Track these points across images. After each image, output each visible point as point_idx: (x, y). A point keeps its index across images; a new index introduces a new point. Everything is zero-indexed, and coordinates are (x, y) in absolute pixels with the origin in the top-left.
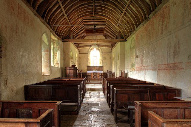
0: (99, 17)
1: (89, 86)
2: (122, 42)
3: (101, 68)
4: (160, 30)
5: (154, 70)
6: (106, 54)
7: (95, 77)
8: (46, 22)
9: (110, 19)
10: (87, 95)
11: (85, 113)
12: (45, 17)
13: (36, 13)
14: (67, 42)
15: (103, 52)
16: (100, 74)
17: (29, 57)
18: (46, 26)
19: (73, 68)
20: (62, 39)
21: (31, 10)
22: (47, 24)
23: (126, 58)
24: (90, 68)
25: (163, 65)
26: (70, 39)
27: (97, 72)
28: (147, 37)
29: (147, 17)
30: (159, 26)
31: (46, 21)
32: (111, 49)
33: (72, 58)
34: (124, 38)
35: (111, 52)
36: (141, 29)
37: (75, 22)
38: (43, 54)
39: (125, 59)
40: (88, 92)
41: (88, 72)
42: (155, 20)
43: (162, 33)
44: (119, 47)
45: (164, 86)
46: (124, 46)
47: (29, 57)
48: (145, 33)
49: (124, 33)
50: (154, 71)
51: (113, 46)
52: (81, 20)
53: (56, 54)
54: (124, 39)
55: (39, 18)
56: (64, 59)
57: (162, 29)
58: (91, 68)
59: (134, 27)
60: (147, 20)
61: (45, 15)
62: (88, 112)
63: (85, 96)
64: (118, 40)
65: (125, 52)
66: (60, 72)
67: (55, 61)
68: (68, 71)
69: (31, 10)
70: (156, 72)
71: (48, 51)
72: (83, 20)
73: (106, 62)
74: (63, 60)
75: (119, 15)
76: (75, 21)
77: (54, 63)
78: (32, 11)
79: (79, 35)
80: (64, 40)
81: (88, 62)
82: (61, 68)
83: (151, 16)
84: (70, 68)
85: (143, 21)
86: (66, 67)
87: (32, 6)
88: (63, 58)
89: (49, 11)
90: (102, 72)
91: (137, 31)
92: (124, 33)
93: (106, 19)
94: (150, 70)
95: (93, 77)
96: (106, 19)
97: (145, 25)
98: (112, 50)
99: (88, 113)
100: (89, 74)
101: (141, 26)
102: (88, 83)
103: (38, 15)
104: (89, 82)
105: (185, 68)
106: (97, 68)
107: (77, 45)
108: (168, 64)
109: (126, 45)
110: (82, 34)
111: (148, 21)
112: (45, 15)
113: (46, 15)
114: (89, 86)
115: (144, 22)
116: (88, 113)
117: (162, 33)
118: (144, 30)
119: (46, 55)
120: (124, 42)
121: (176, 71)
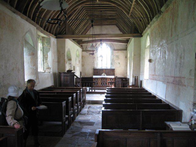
0: (105, 3)
1: (89, 97)
2: (137, 38)
3: (111, 71)
4: (170, 31)
5: (164, 82)
6: (120, 52)
7: (104, 84)
8: (29, 19)
9: (119, 5)
10: (85, 110)
11: (72, 135)
12: (28, 12)
13: (15, 10)
14: (62, 39)
15: (116, 48)
16: (110, 80)
17: (6, 67)
18: (30, 23)
19: (69, 75)
20: (55, 35)
21: (8, 8)
22: (32, 21)
23: (141, 60)
24: (97, 72)
25: (171, 77)
26: (66, 34)
27: (106, 76)
28: (159, 37)
29: (159, 9)
30: (169, 25)
31: (29, 17)
32: (127, 45)
33: (70, 59)
34: (140, 32)
35: (127, 48)
36: (154, 24)
37: (72, 12)
38: (27, 58)
39: (140, 61)
40: (88, 106)
41: (94, 77)
42: (166, 15)
43: (172, 35)
44: (133, 44)
45: (168, 104)
46: (140, 42)
47: (6, 67)
48: (158, 30)
49: (138, 24)
50: (164, 84)
51: (127, 41)
52: (81, 8)
53: (46, 57)
54: (139, 33)
55: (19, 15)
56: (59, 62)
57: (172, 30)
58: (99, 70)
59: (148, 20)
60: (160, 14)
61: (28, 10)
62: (76, 133)
63: (81, 112)
64: (132, 35)
65: (140, 52)
66: (53, 79)
67: (46, 65)
68: (62, 77)
69: (9, 9)
70: (166, 85)
71: (34, 54)
72: (84, 7)
73: (119, 63)
74: (56, 63)
75: (130, 2)
76: (72, 10)
77: (43, 68)
78: (10, 10)
79: (81, 27)
80: (58, 35)
81: (94, 62)
82: (54, 74)
83: (163, 9)
84: (65, 75)
85: (156, 14)
86: (59, 73)
87: (10, 3)
88: (56, 60)
89: (29, 11)
90: (113, 77)
91: (152, 25)
92: (138, 24)
93: (114, 5)
94: (161, 81)
95: (102, 84)
96: (114, 5)
97: (159, 19)
98: (128, 45)
99: (75, 135)
100: (95, 80)
101: (154, 19)
102: (89, 93)
103: (17, 11)
104: (93, 91)
105: (186, 86)
106: (108, 71)
107: (79, 42)
108: (174, 77)
109: (141, 42)
110: (85, 25)
111: (162, 16)
112: (28, 10)
113: (30, 8)
114: (89, 97)
115: (157, 16)
116: (75, 135)
117: (172, 35)
118: (157, 26)
119: (32, 59)
120: (139, 38)
121: (180, 87)
